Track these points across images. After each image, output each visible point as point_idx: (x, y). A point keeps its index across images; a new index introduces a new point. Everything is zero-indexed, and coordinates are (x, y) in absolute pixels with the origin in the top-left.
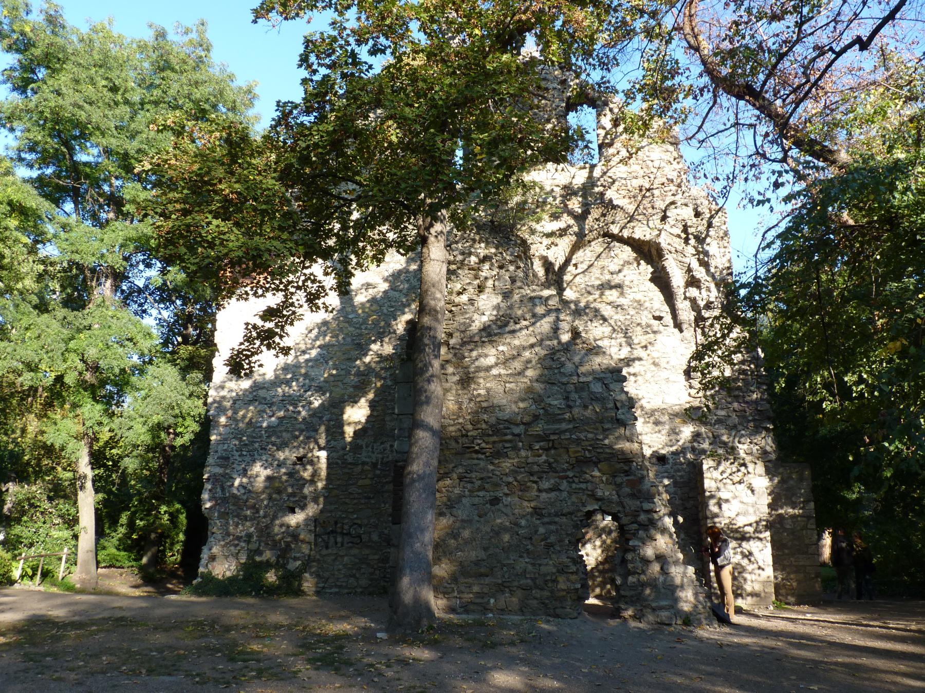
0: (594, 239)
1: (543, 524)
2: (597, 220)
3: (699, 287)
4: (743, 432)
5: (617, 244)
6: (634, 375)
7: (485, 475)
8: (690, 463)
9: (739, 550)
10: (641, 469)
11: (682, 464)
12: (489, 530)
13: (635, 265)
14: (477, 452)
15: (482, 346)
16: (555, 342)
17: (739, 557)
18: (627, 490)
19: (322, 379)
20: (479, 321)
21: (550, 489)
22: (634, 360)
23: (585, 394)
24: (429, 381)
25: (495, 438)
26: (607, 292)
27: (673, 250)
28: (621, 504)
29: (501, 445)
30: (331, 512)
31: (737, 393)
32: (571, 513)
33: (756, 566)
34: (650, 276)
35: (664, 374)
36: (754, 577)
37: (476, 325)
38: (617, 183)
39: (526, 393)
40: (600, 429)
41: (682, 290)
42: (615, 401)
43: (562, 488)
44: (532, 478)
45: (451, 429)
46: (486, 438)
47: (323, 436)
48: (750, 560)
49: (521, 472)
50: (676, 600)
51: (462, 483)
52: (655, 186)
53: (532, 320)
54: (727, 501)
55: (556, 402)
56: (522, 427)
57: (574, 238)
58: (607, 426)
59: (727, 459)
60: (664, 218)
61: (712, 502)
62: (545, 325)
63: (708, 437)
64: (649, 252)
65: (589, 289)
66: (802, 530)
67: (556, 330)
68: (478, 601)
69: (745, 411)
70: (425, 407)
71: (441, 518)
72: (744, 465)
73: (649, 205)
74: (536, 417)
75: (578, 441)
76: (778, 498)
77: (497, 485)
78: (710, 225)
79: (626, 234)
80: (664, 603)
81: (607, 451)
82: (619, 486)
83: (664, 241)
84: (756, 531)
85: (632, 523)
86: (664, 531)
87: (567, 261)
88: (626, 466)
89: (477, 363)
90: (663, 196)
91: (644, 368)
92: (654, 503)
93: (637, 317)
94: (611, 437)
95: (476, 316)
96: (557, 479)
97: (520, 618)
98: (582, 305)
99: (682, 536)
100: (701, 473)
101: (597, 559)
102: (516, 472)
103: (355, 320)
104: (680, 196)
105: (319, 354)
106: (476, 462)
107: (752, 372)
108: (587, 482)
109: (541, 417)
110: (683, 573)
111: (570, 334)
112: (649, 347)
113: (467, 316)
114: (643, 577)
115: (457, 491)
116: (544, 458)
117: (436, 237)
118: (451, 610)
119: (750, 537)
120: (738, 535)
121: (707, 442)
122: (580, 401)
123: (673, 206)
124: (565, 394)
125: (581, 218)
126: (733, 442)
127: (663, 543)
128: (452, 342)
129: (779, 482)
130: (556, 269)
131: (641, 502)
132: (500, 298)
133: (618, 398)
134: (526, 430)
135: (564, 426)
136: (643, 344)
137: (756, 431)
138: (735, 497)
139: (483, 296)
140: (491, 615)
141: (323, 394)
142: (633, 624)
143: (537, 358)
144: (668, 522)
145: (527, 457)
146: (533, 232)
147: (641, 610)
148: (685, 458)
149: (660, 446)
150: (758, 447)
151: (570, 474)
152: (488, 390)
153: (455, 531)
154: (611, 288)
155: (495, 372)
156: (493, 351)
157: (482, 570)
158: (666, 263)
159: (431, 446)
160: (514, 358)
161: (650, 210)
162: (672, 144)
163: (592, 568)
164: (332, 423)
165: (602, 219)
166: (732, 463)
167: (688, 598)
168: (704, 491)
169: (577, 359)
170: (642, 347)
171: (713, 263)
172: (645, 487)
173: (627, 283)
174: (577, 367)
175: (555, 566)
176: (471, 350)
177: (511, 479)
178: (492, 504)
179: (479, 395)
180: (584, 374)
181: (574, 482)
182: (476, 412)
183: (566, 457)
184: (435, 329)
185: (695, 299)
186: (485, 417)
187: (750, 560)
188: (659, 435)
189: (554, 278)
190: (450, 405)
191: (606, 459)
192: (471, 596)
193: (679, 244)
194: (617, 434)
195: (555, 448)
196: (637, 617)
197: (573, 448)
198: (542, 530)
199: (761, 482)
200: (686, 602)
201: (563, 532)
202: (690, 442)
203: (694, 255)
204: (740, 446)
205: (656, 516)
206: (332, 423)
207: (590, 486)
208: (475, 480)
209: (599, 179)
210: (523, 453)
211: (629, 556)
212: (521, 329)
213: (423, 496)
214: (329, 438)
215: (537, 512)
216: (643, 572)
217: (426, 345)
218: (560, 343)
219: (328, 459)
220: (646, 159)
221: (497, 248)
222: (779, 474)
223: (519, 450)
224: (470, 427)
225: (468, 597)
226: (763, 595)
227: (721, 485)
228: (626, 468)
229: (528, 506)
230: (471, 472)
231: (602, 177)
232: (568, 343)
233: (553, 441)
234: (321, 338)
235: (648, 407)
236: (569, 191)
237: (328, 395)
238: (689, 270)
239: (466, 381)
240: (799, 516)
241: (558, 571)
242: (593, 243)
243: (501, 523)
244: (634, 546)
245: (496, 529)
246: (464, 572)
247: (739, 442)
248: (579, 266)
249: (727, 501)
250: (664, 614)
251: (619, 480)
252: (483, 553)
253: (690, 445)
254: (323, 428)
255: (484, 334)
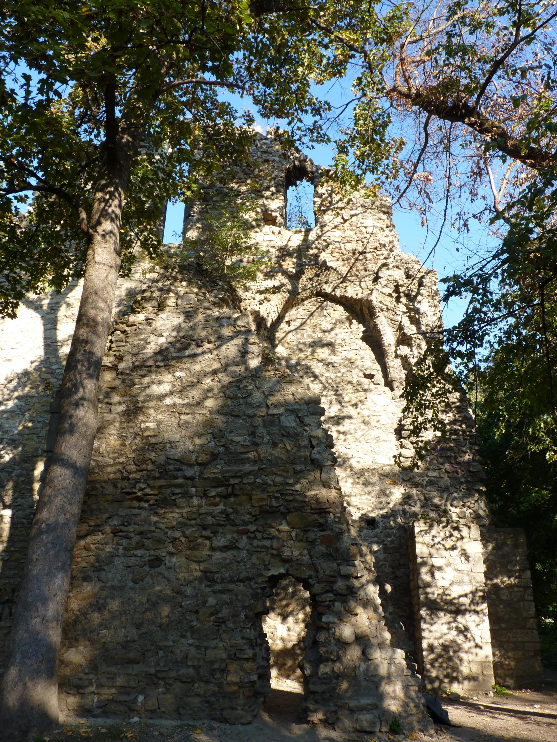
0: (307, 298)
1: (214, 592)
2: (311, 279)
3: (410, 345)
4: (455, 495)
5: (330, 304)
6: (344, 433)
7: (145, 528)
8: (400, 527)
9: (454, 625)
10: (339, 522)
11: (391, 528)
12: (144, 600)
13: (347, 324)
14: (139, 499)
15: (156, 372)
16: (242, 368)
17: (454, 633)
18: (322, 549)
19: (16, 432)
20: (155, 343)
21: (225, 547)
22: (343, 418)
23: (275, 429)
24: (77, 405)
25: (162, 482)
26: (319, 350)
27: (384, 308)
28: (313, 566)
29: (169, 490)
30: (9, 578)
31: (449, 453)
32: (249, 579)
33: (472, 644)
34: (361, 335)
35: (374, 433)
36: (471, 657)
37: (150, 350)
38: (331, 246)
39: (204, 427)
40: (291, 471)
41: (393, 348)
42: (310, 437)
43: (240, 545)
44: (204, 533)
45: (109, 469)
46: (151, 482)
47: (10, 493)
48: (466, 637)
49: (191, 526)
50: (381, 697)
51: (116, 539)
52: (368, 250)
53: (218, 343)
54: (440, 569)
55: (239, 439)
56: (196, 468)
57: (287, 295)
58: (298, 468)
59: (439, 522)
60: (376, 279)
61: (424, 570)
62: (231, 349)
63: (419, 500)
64: (360, 311)
65: (300, 346)
66: (519, 601)
67: (244, 353)
68: (122, 698)
69: (457, 473)
70: (68, 437)
71: (85, 584)
72: (457, 529)
73: (362, 268)
74: (214, 457)
75: (264, 487)
76: (493, 567)
77: (159, 541)
78: (421, 284)
79: (338, 293)
80: (364, 701)
81: (298, 498)
82: (312, 543)
83: (375, 298)
84: (472, 602)
85: (327, 592)
86: (367, 603)
87: (280, 319)
88: (324, 523)
89: (148, 391)
90: (376, 259)
91: (355, 427)
92: (354, 566)
93: (348, 374)
94: (304, 481)
95: (152, 338)
96: (235, 535)
97: (173, 723)
98: (293, 362)
99: (391, 609)
100: (412, 537)
101: (299, 634)
102: (185, 525)
103: (58, 371)
104: (392, 259)
105: (16, 405)
106: (136, 511)
107: (464, 432)
108: (272, 538)
109: (221, 456)
110: (390, 660)
111: (260, 359)
112: (360, 405)
113: (142, 337)
114: (338, 667)
115: (108, 549)
116: (221, 507)
117: (103, 236)
118: (83, 711)
119: (466, 610)
120: (453, 608)
121: (419, 505)
122: (271, 442)
123: (385, 268)
124: (251, 429)
125: (294, 278)
126: (446, 505)
127: (364, 619)
128: (122, 366)
129: (493, 549)
130: (269, 325)
131: (339, 565)
132: (181, 318)
133: (314, 434)
134: (202, 473)
135: (248, 467)
136: (354, 402)
137: (469, 494)
138: (449, 565)
139: (163, 315)
140: (136, 719)
141: (15, 448)
142: (324, 732)
143: (220, 385)
144: (373, 591)
145: (200, 506)
146: (247, 289)
147: (335, 712)
148: (395, 522)
149: (370, 509)
150: (470, 511)
151: (252, 528)
152: (159, 423)
153: (101, 601)
154: (323, 346)
155: (168, 401)
156: (168, 377)
157: (131, 655)
158: (377, 321)
159: (70, 487)
160: (193, 385)
161: (363, 273)
162: (384, 213)
163: (294, 645)
164: (22, 479)
165: (316, 279)
166: (444, 527)
167: (395, 696)
168: (416, 557)
169: (266, 387)
170: (353, 405)
171: (424, 321)
172: (344, 546)
173: (339, 341)
174: (266, 397)
175: (226, 649)
176: (143, 376)
177: (178, 534)
178: (151, 567)
179: (148, 428)
180: (275, 406)
181: (255, 538)
182: (142, 450)
183: (248, 507)
184: (92, 344)
185: (406, 356)
186: (152, 455)
187: (466, 637)
188: (369, 497)
189: (266, 334)
190: (110, 441)
191: (297, 509)
192: (114, 691)
193: (390, 302)
194: (311, 478)
195: (236, 495)
196: (329, 723)
197: (257, 494)
198: (212, 601)
199: (476, 548)
200: (394, 698)
201: (239, 604)
202: (401, 504)
203: (405, 313)
204: (453, 509)
205: (356, 583)
206: (22, 479)
207: (275, 544)
208: (132, 535)
209: (314, 242)
210: (195, 501)
211: (322, 637)
212: (203, 353)
213: (51, 553)
214: (16, 495)
215: (208, 576)
216: (339, 659)
217: (79, 361)
218: (247, 369)
219: (13, 517)
220: (359, 225)
221: (200, 288)
222: (494, 539)
223: (191, 497)
224: (133, 468)
225: (108, 693)
226: (481, 678)
227: (433, 551)
228: (321, 521)
229: (196, 570)
230: (129, 524)
231: (317, 240)
232: (258, 369)
233: (233, 485)
234: (20, 389)
235: (357, 466)
236: (284, 252)
237: (20, 449)
238: (401, 328)
239: (134, 411)
240: (515, 585)
241: (229, 657)
242: (306, 302)
243: (161, 591)
244: (328, 623)
245: (154, 599)
246: (106, 659)
247: (452, 505)
248: (292, 323)
249: (440, 569)
250: (365, 719)
251: (311, 536)
252: (134, 631)
253: (401, 508)
254: (10, 484)
255: (159, 357)
